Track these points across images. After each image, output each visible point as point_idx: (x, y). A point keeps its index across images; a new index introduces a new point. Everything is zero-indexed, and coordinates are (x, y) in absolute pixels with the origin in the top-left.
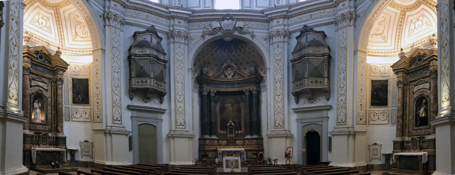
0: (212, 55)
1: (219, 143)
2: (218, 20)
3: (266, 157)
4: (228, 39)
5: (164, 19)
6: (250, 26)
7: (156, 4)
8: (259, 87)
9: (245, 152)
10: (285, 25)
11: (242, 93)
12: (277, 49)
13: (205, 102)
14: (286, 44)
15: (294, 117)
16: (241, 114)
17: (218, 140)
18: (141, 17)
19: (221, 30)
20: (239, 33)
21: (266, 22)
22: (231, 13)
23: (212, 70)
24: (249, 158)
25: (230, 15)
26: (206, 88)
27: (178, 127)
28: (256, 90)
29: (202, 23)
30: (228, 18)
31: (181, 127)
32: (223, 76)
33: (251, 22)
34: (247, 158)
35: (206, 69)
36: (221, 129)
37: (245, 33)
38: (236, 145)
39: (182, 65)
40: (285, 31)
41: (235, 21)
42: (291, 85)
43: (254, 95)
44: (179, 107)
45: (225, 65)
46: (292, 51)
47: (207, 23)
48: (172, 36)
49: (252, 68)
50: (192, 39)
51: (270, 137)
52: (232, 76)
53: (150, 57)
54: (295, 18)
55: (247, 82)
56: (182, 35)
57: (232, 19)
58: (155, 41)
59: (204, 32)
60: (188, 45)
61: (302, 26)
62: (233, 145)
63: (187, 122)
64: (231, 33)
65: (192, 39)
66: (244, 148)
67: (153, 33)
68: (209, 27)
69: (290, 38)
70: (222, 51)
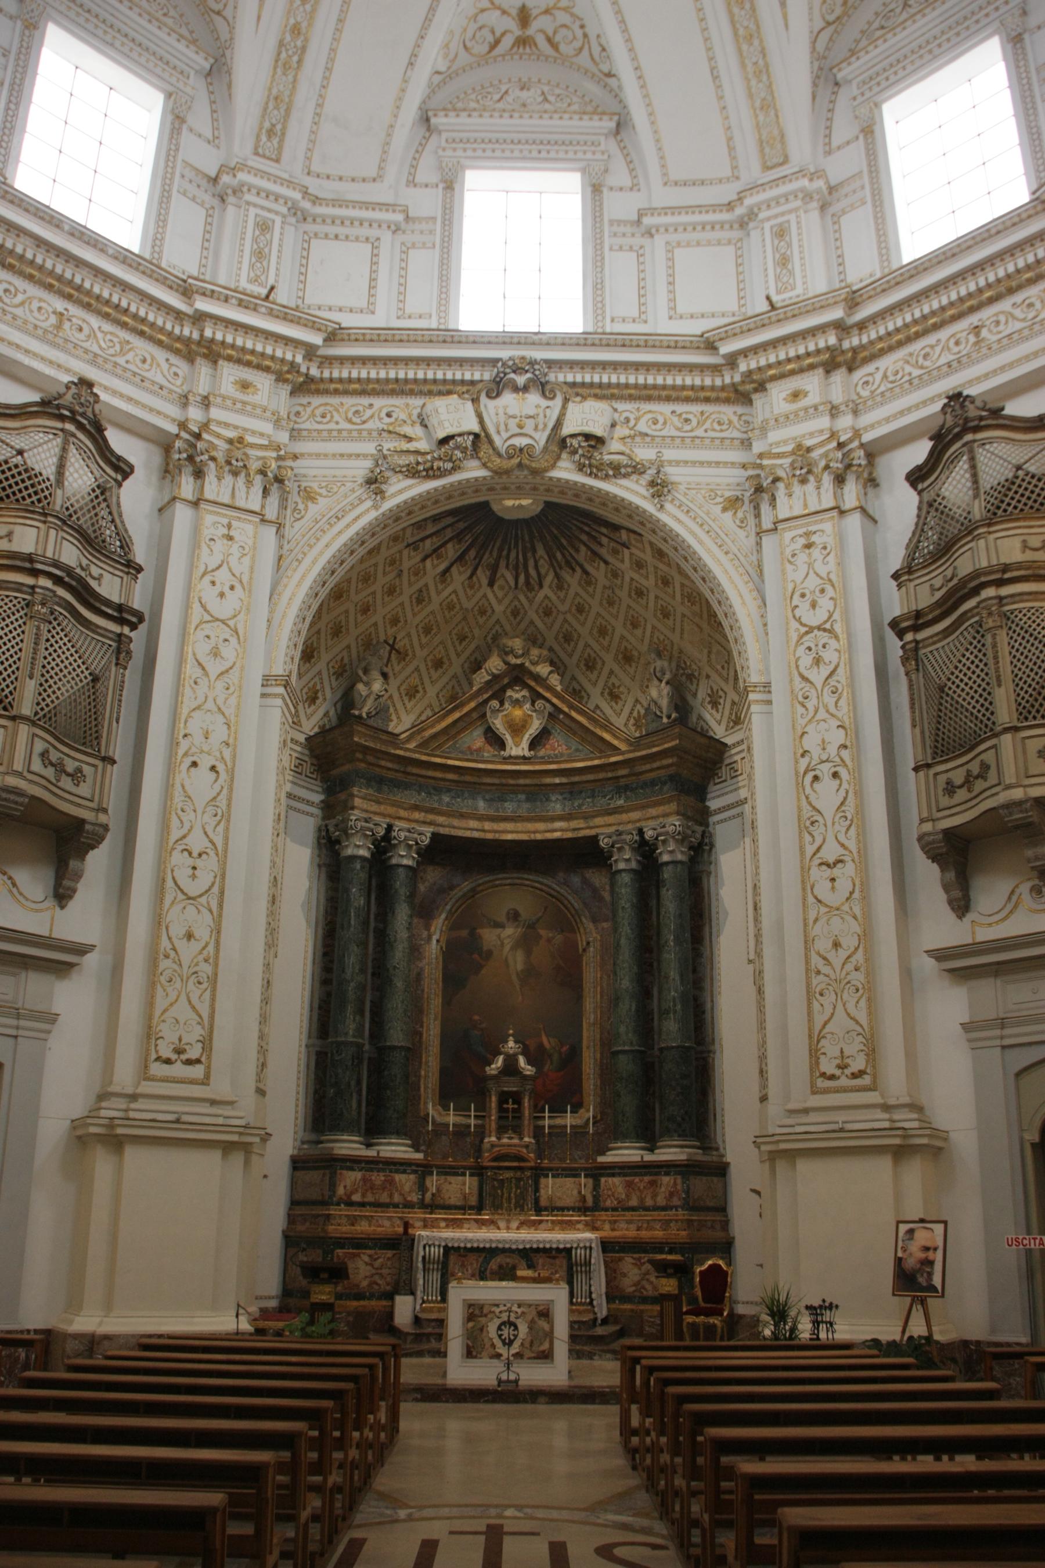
0: (420, 598)
1: (422, 1188)
2: (470, 390)
3: (747, 1291)
4: (516, 505)
5: (161, 355)
6: (642, 427)
7: (123, 257)
8: (701, 816)
9: (597, 1258)
10: (834, 411)
11: (586, 854)
12: (802, 558)
13: (357, 899)
14: (854, 521)
15: (949, 1007)
16: (579, 998)
17: (423, 1170)
18: (19, 312)
19: (485, 449)
20: (581, 468)
21: (727, 401)
22: (539, 355)
23: (412, 693)
24: (626, 1299)
25: (533, 363)
26: (367, 812)
27: (157, 1069)
28: (682, 839)
29: (379, 402)
30: (521, 380)
31: (179, 1070)
32: (476, 739)
33: (646, 406)
34: (610, 1298)
35: (377, 686)
36: (445, 1098)
37: (617, 471)
38: (539, 1210)
39: (229, 652)
40: (840, 446)
41: (558, 401)
42: (910, 783)
43: (667, 874)
44: (177, 930)
45: (495, 664)
46: (896, 560)
47: (404, 407)
48: (190, 458)
49: (654, 693)
50: (309, 496)
51: (781, 1154)
52: (533, 744)
53: (35, 573)
54: (887, 363)
55: (623, 781)
56: (254, 466)
57: (545, 389)
58: (81, 477)
59: (381, 457)
60: (280, 527)
61: (933, 400)
62: (520, 1207)
63: (219, 1042)
64: (535, 472)
65: (309, 496)
66: (594, 1229)
67: (80, 426)
68: (418, 431)
69: (872, 482)
70: (483, 576)
